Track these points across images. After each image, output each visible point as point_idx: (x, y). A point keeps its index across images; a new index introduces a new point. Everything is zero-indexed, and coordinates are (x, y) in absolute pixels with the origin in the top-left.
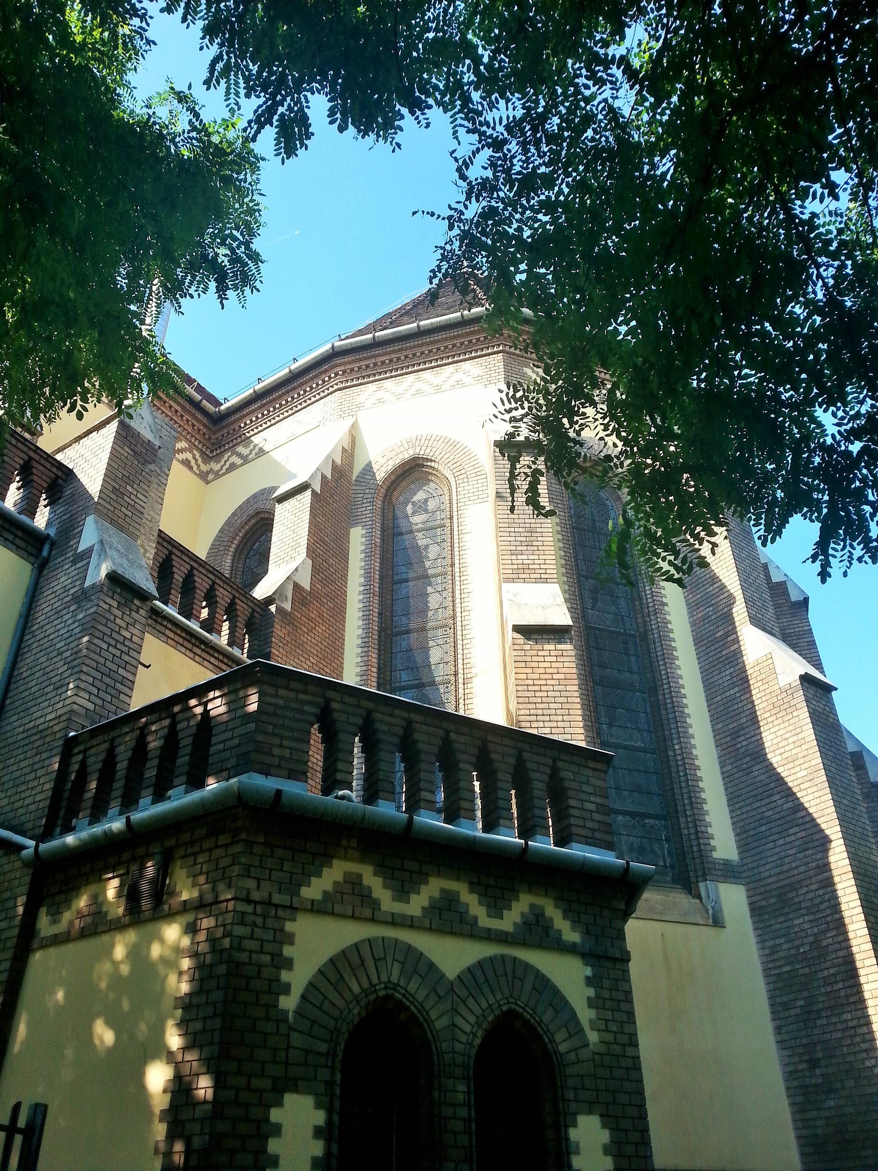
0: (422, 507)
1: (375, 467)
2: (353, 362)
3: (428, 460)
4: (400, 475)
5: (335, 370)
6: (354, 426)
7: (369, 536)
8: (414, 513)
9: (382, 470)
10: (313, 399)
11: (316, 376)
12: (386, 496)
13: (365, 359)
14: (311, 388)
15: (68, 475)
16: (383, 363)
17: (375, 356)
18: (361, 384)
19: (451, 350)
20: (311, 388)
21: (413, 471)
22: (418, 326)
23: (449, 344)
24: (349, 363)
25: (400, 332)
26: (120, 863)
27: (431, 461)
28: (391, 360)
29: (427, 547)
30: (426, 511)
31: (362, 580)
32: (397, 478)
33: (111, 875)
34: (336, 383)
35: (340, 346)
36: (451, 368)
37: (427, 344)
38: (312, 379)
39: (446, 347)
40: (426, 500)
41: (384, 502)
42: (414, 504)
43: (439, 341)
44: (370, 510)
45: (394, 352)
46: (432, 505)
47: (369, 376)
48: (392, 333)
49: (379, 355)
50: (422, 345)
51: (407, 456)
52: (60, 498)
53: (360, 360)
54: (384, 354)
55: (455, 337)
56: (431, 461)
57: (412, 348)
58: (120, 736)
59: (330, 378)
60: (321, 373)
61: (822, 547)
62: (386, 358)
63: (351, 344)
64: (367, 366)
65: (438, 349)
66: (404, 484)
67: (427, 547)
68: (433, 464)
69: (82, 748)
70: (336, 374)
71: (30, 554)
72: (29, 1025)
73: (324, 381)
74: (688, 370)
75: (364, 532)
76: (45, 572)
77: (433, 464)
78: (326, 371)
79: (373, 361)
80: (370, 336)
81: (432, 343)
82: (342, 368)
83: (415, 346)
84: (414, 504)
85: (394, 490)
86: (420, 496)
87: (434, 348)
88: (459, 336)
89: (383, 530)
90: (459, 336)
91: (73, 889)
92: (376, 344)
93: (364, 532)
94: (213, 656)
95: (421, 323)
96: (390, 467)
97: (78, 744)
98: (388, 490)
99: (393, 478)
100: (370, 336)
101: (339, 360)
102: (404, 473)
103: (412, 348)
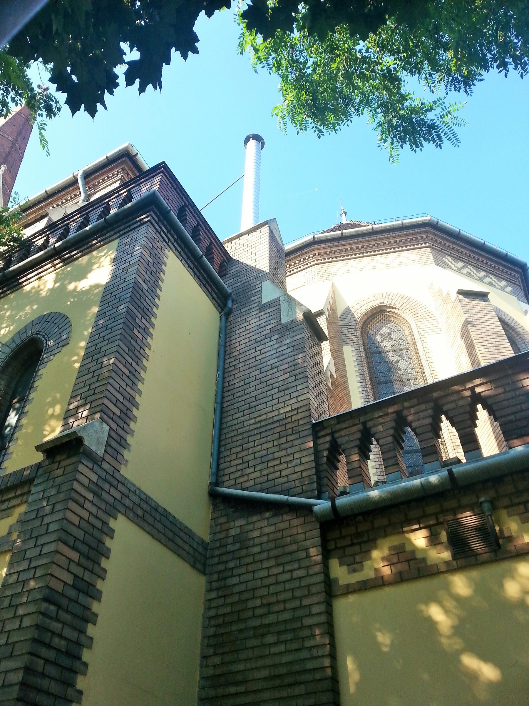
0: (388, 337)
1: (353, 310)
2: (326, 248)
3: (390, 307)
4: (371, 317)
5: (313, 252)
6: (333, 284)
7: (357, 351)
8: (382, 341)
9: (359, 312)
10: (296, 271)
11: (299, 256)
12: (362, 329)
13: (334, 246)
15: (229, 261)
17: (341, 245)
18: (332, 262)
20: (295, 263)
21: (379, 314)
23: (392, 241)
24: (323, 248)
25: (360, 231)
26: (425, 516)
27: (393, 308)
28: (352, 249)
29: (397, 362)
30: (391, 339)
31: (359, 379)
32: (368, 319)
33: (417, 526)
34: (313, 261)
35: (319, 238)
36: (395, 254)
37: (377, 240)
38: (296, 258)
39: (390, 243)
40: (390, 334)
41: (361, 332)
42: (381, 335)
43: (385, 238)
44: (355, 336)
45: (354, 243)
46: (394, 336)
47: (336, 258)
48: (355, 231)
50: (374, 240)
51: (375, 304)
52: (226, 274)
53: (331, 247)
54: (347, 244)
55: (396, 237)
56: (393, 308)
57: (366, 241)
58: (372, 419)
59: (309, 257)
60: (303, 254)
63: (326, 236)
64: (336, 251)
65: (384, 243)
66: (373, 322)
67: (397, 362)
68: (393, 310)
69: (329, 431)
70: (314, 255)
71: (219, 305)
72: (361, 666)
75: (353, 349)
77: (393, 310)
78: (306, 253)
79: (340, 248)
81: (380, 239)
82: (318, 251)
84: (381, 335)
85: (368, 325)
86: (384, 330)
88: (398, 236)
89: (365, 349)
90: (398, 236)
91: (369, 541)
92: (342, 238)
93: (353, 349)
94: (9, 500)
97: (324, 428)
98: (363, 325)
99: (366, 317)
101: (316, 246)
102: (373, 315)
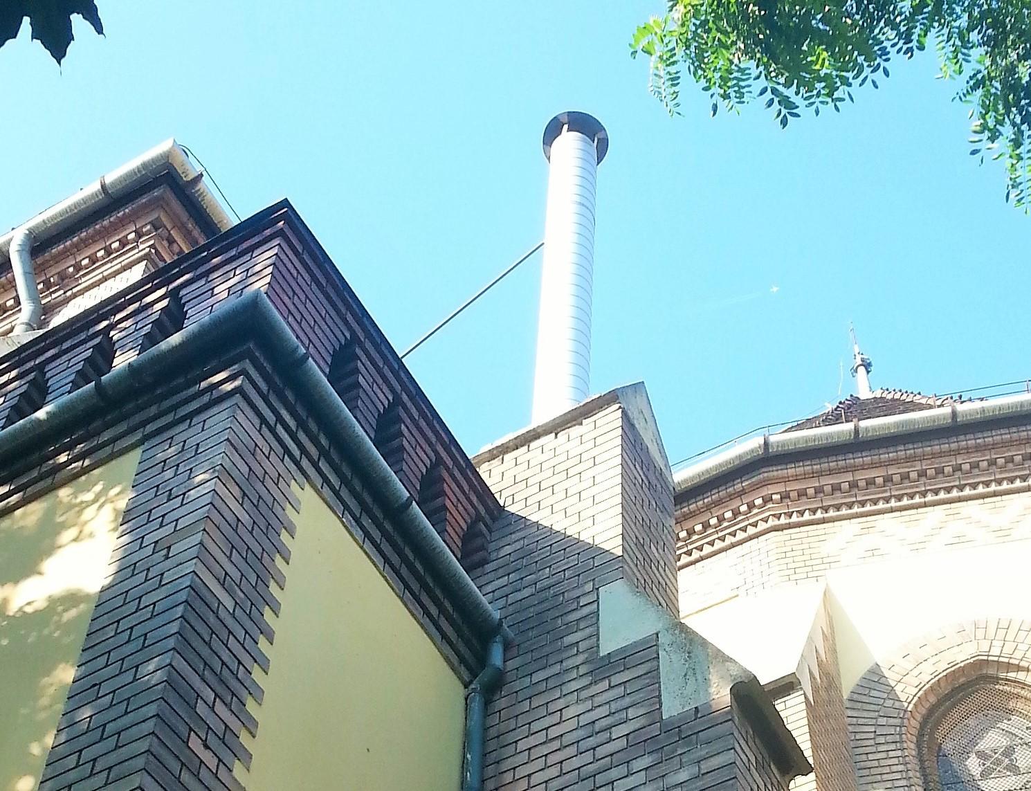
4: (947, 697)
5: (766, 491)
9: (910, 683)
13: (831, 472)
14: (706, 526)
16: (870, 482)
17: (854, 469)
19: (1003, 468)
20: (706, 526)
22: (856, 430)
24: (796, 478)
32: (940, 703)
34: (764, 517)
37: (968, 450)
38: (708, 508)
42: (982, 755)
43: (994, 446)
48: (897, 424)
49: (863, 467)
50: (957, 452)
51: (963, 655)
53: (820, 474)
57: (934, 456)
59: (751, 506)
60: (731, 497)
61: (1029, 158)
62: (877, 474)
63: (807, 440)
65: (992, 463)
66: (955, 714)
70: (767, 500)
73: (736, 513)
74: (765, 45)
76: (501, 703)
80: (848, 427)
81: (978, 449)
82: (781, 488)
83: (941, 454)
84: (982, 755)
87: (983, 459)
92: (858, 444)
95: (864, 424)
96: (926, 677)
98: (923, 724)
99: (933, 699)
100: (848, 427)
102: (955, 691)
103: (934, 456)
